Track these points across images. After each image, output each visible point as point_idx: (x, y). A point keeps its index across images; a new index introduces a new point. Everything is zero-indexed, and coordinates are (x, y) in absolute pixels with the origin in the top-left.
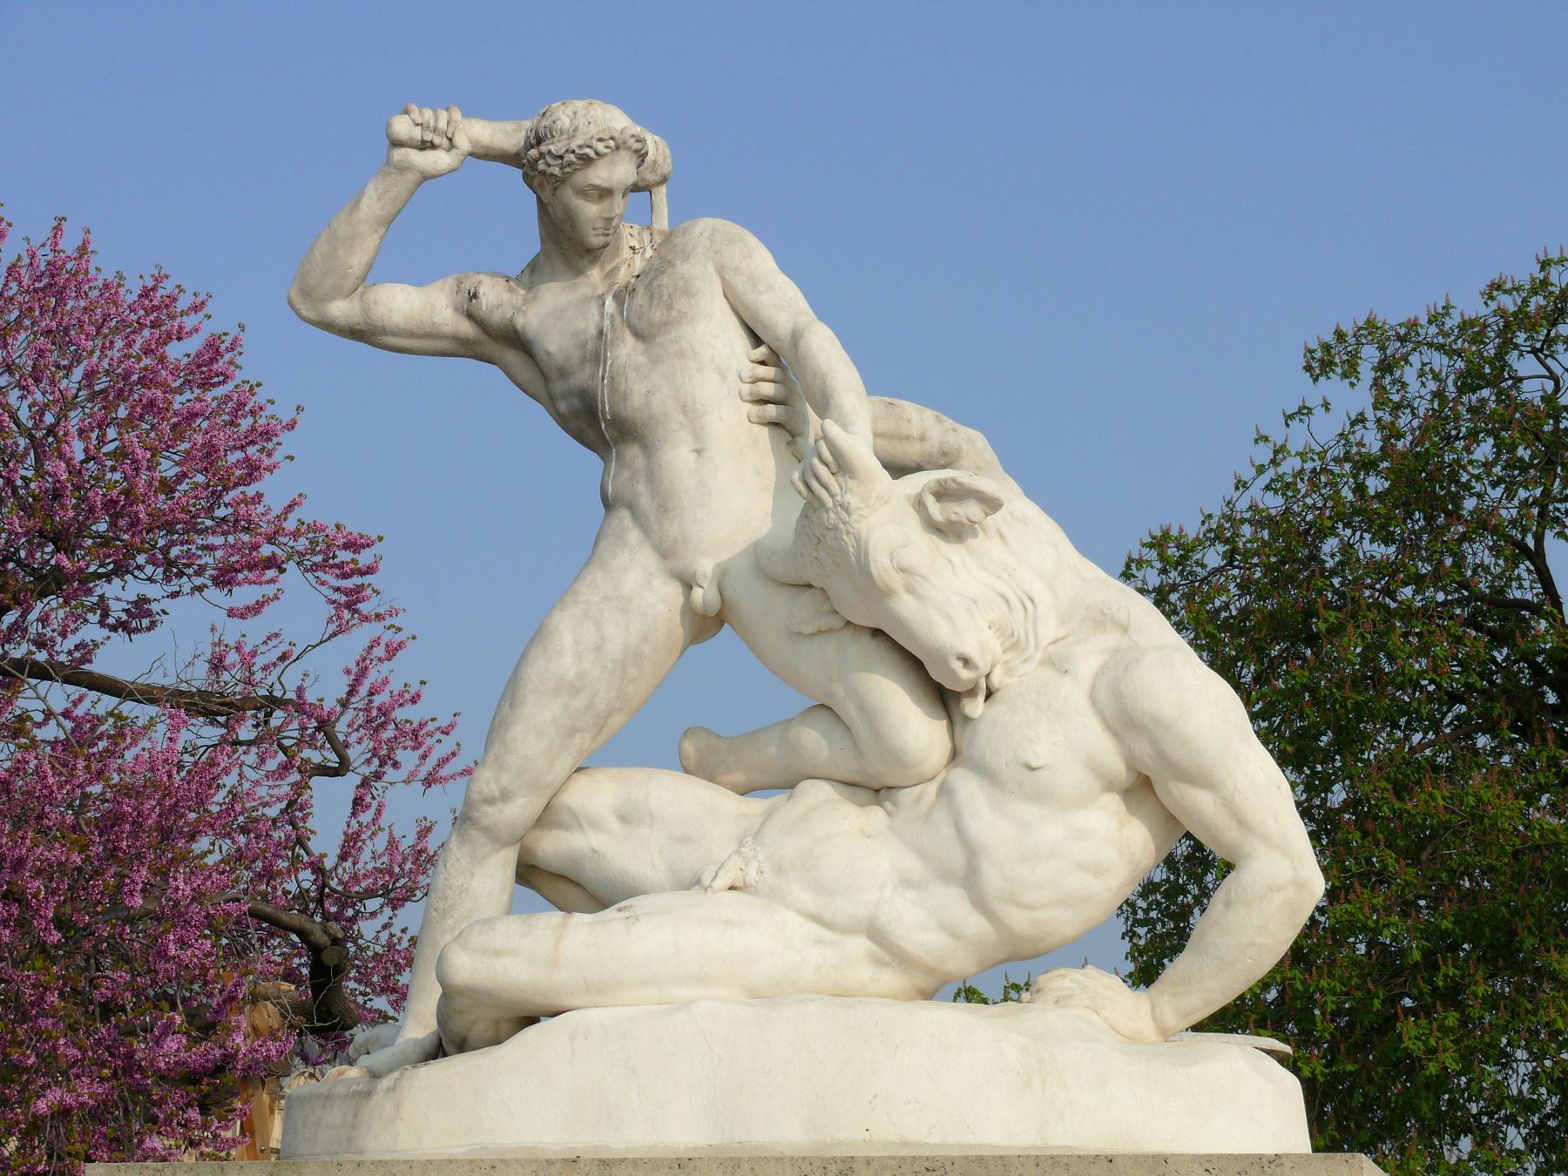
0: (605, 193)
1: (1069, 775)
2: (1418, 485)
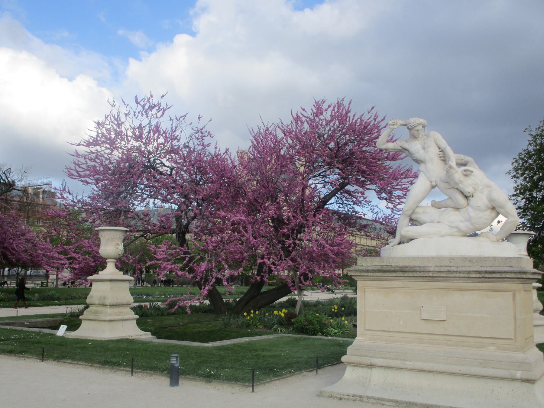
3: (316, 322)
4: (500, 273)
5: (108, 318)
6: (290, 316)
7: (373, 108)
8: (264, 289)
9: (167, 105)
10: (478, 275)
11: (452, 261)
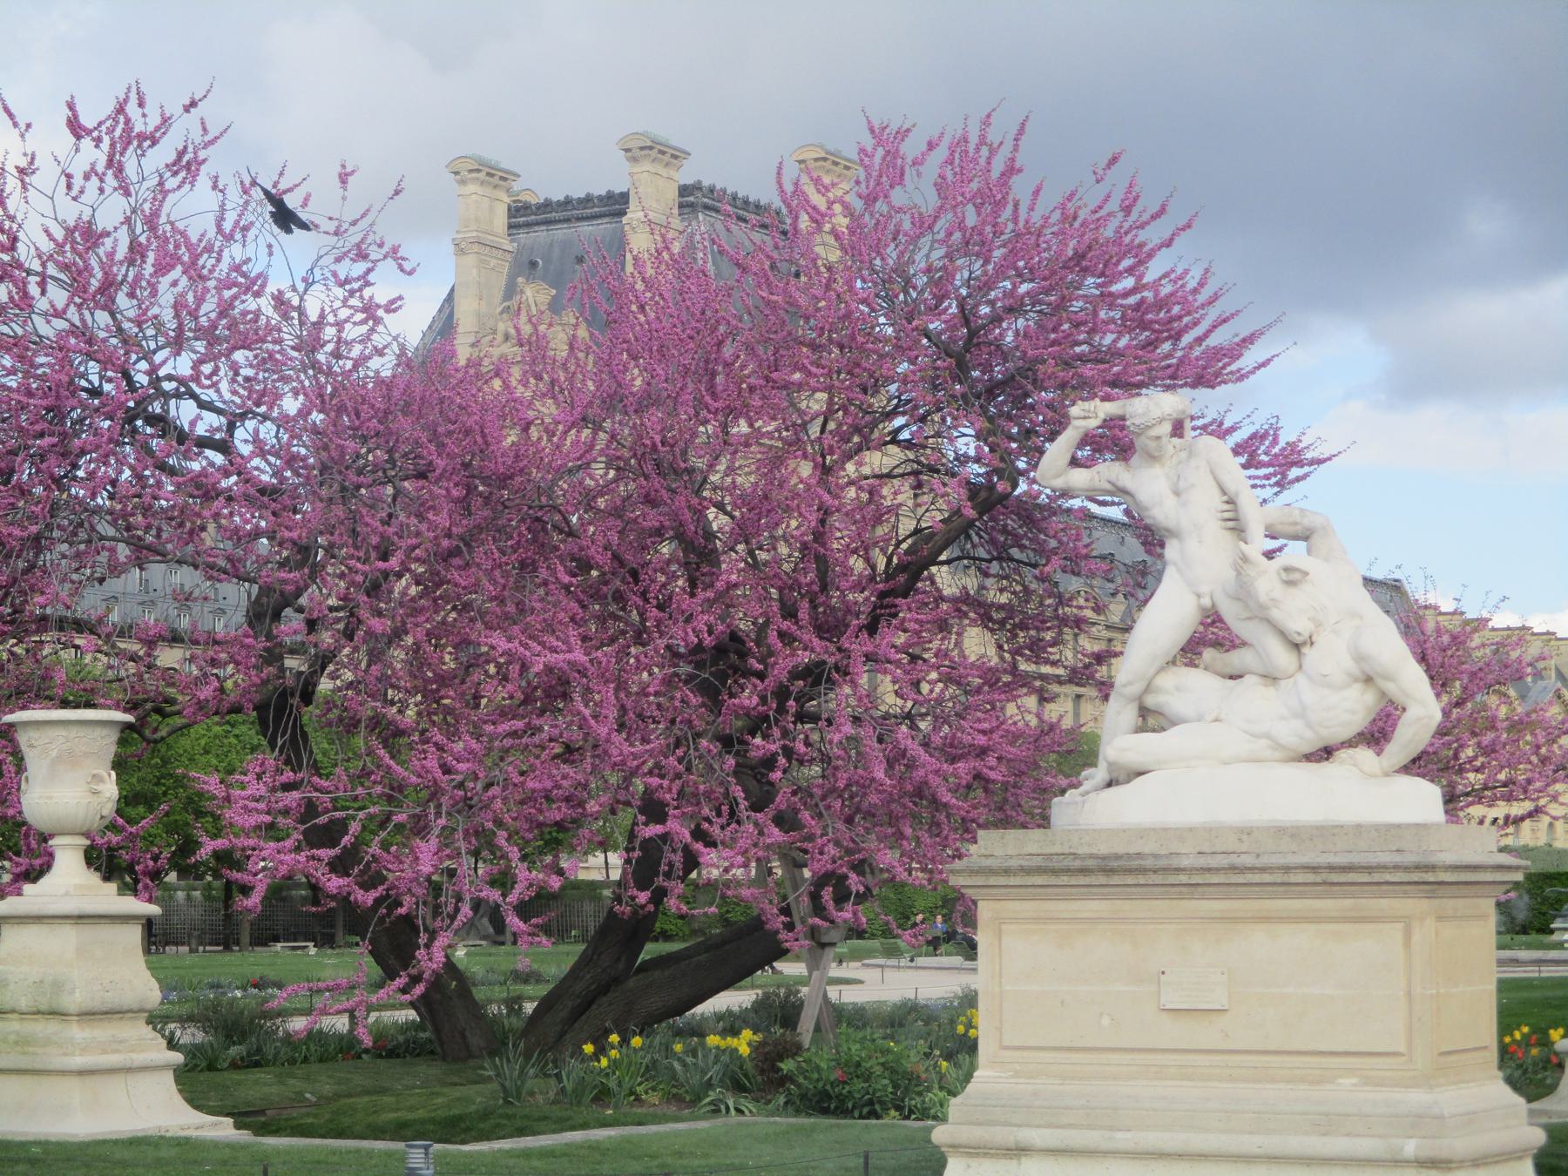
3: (878, 1070)
4: (1369, 869)
5: (78, 1061)
6: (769, 1058)
7: (1114, 160)
8: (650, 950)
9: (205, 129)
10: (1310, 878)
11: (1245, 837)
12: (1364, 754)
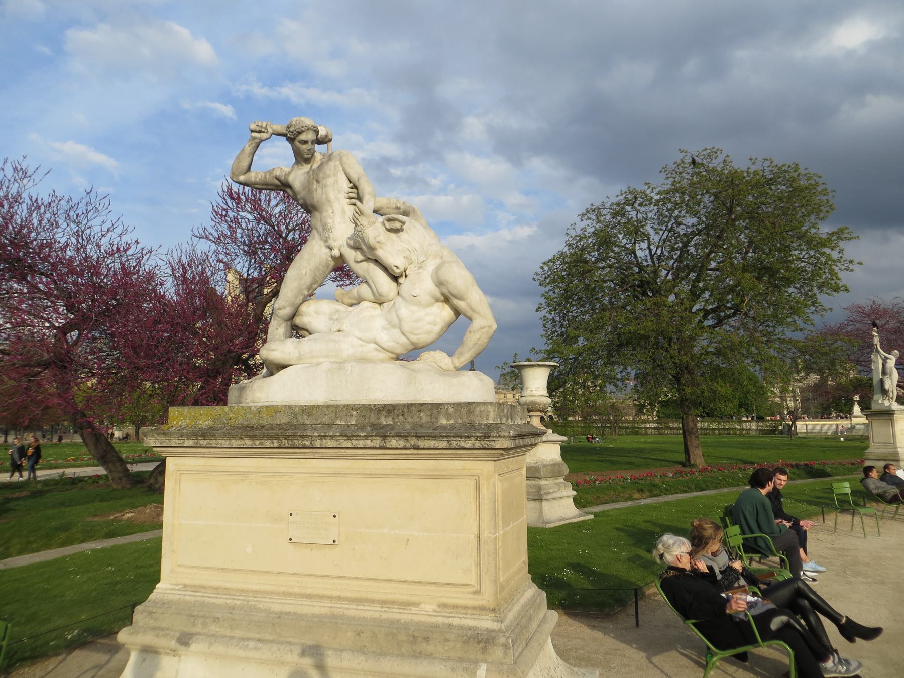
0: (306, 142)
1: (426, 298)
2: (604, 241)
12: (440, 357)
